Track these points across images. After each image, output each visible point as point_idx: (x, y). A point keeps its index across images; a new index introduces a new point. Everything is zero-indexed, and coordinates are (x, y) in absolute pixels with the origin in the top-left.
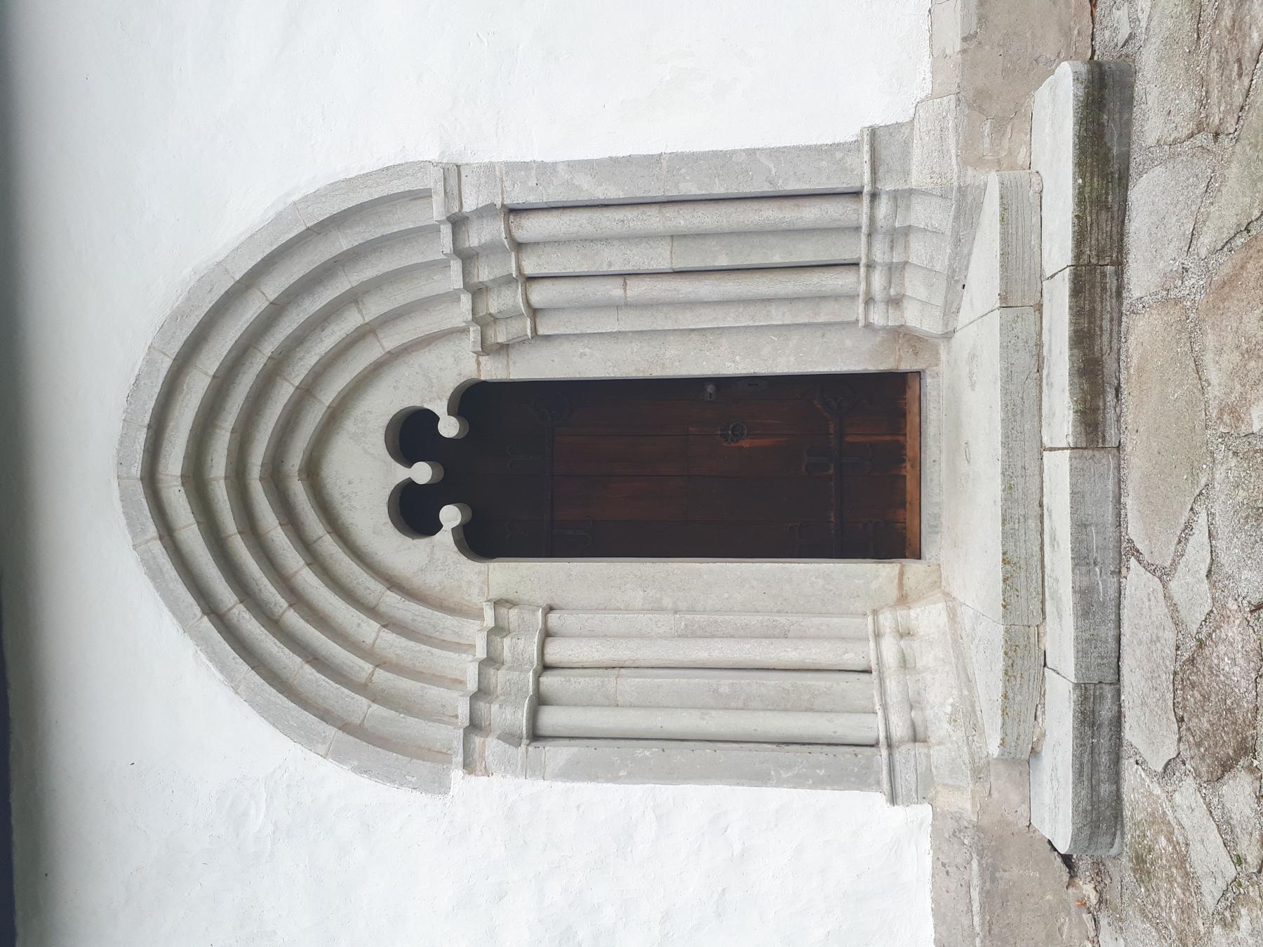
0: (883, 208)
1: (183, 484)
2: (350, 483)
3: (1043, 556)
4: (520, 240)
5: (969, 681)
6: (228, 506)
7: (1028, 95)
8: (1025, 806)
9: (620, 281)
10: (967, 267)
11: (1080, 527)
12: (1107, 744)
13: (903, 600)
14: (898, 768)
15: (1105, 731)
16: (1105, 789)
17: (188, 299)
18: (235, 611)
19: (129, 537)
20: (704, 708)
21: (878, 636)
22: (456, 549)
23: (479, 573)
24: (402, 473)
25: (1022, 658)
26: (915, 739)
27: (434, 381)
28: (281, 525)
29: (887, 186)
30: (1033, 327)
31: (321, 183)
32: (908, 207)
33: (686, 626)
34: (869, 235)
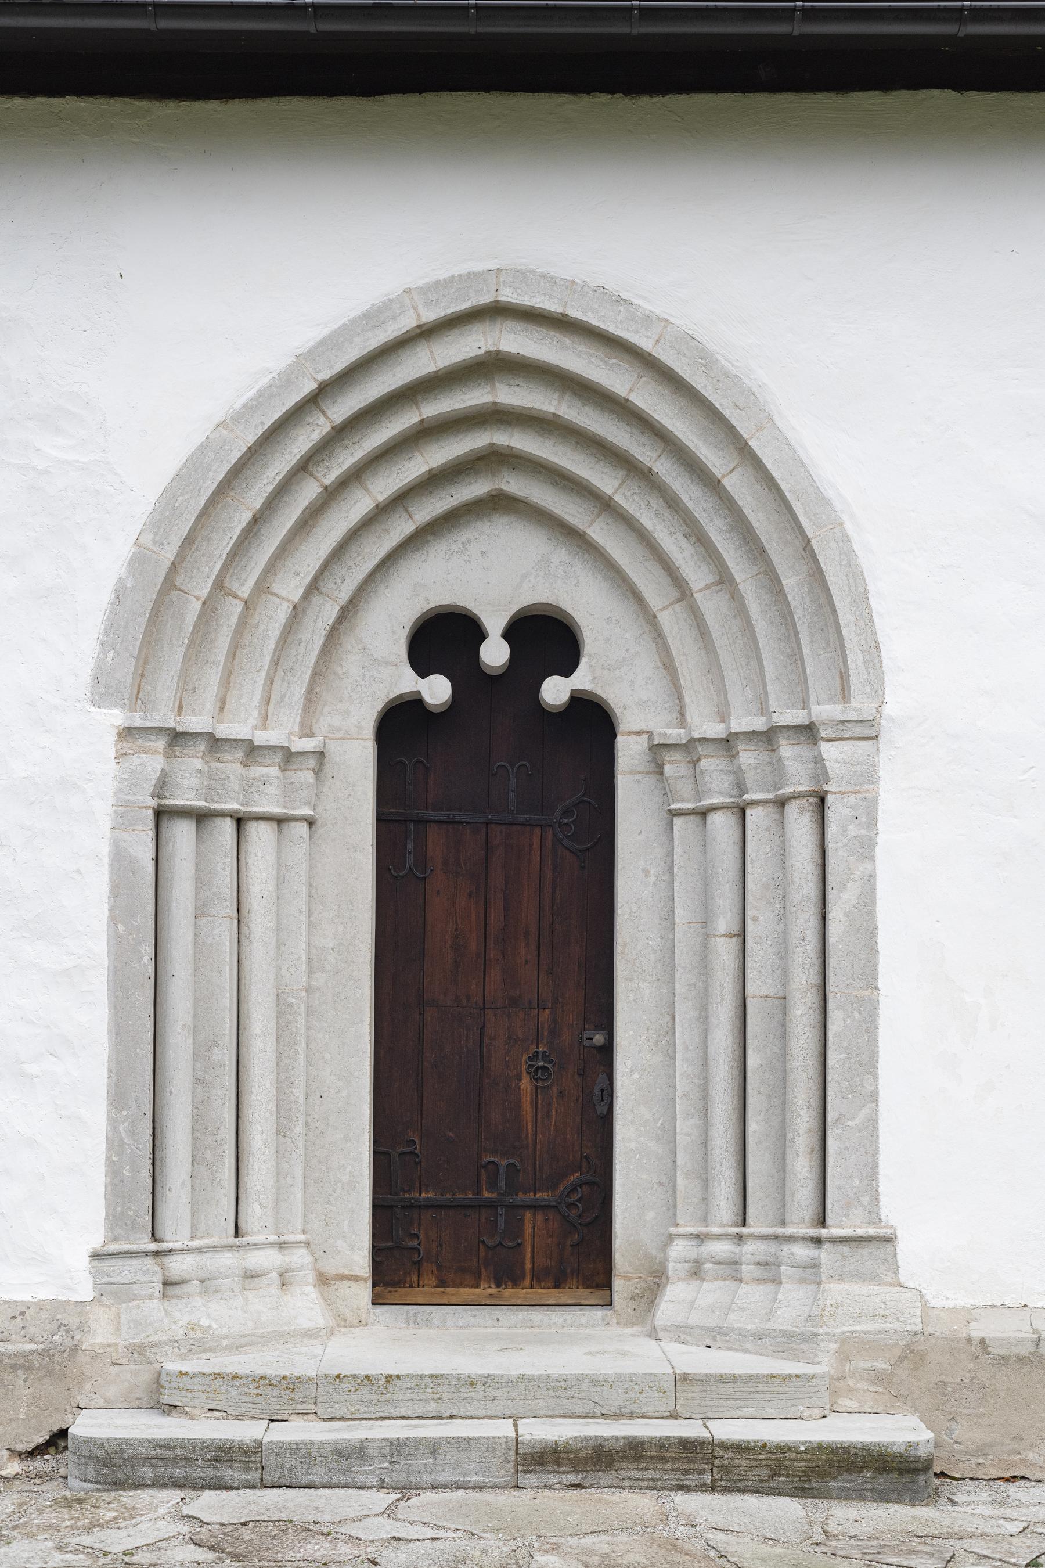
0: (802, 1252)
1: (488, 352)
2: (483, 553)
3: (394, 1419)
4: (786, 807)
5: (237, 1348)
6: (457, 406)
7: (915, 1409)
8: (101, 1402)
9: (736, 929)
10: (730, 1349)
11: (434, 1447)
12: (196, 1475)
13: (324, 1280)
14: (135, 1262)
15: (211, 1473)
16: (147, 1473)
17: (727, 375)
18: (322, 420)
19: (421, 283)
20: (196, 1030)
21: (281, 1246)
22: (392, 696)
23: (360, 728)
24: (495, 624)
25: (286, 1393)
26: (166, 1284)
27: (617, 673)
28: (430, 471)
29: (825, 1255)
30: (652, 1409)
31: (865, 561)
32: (803, 1281)
33: (291, 1005)
34: (776, 1237)
